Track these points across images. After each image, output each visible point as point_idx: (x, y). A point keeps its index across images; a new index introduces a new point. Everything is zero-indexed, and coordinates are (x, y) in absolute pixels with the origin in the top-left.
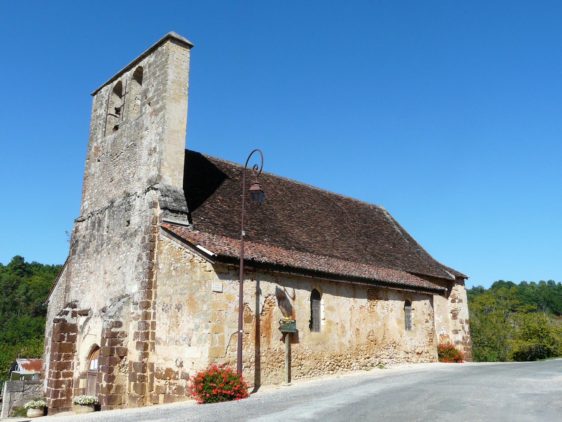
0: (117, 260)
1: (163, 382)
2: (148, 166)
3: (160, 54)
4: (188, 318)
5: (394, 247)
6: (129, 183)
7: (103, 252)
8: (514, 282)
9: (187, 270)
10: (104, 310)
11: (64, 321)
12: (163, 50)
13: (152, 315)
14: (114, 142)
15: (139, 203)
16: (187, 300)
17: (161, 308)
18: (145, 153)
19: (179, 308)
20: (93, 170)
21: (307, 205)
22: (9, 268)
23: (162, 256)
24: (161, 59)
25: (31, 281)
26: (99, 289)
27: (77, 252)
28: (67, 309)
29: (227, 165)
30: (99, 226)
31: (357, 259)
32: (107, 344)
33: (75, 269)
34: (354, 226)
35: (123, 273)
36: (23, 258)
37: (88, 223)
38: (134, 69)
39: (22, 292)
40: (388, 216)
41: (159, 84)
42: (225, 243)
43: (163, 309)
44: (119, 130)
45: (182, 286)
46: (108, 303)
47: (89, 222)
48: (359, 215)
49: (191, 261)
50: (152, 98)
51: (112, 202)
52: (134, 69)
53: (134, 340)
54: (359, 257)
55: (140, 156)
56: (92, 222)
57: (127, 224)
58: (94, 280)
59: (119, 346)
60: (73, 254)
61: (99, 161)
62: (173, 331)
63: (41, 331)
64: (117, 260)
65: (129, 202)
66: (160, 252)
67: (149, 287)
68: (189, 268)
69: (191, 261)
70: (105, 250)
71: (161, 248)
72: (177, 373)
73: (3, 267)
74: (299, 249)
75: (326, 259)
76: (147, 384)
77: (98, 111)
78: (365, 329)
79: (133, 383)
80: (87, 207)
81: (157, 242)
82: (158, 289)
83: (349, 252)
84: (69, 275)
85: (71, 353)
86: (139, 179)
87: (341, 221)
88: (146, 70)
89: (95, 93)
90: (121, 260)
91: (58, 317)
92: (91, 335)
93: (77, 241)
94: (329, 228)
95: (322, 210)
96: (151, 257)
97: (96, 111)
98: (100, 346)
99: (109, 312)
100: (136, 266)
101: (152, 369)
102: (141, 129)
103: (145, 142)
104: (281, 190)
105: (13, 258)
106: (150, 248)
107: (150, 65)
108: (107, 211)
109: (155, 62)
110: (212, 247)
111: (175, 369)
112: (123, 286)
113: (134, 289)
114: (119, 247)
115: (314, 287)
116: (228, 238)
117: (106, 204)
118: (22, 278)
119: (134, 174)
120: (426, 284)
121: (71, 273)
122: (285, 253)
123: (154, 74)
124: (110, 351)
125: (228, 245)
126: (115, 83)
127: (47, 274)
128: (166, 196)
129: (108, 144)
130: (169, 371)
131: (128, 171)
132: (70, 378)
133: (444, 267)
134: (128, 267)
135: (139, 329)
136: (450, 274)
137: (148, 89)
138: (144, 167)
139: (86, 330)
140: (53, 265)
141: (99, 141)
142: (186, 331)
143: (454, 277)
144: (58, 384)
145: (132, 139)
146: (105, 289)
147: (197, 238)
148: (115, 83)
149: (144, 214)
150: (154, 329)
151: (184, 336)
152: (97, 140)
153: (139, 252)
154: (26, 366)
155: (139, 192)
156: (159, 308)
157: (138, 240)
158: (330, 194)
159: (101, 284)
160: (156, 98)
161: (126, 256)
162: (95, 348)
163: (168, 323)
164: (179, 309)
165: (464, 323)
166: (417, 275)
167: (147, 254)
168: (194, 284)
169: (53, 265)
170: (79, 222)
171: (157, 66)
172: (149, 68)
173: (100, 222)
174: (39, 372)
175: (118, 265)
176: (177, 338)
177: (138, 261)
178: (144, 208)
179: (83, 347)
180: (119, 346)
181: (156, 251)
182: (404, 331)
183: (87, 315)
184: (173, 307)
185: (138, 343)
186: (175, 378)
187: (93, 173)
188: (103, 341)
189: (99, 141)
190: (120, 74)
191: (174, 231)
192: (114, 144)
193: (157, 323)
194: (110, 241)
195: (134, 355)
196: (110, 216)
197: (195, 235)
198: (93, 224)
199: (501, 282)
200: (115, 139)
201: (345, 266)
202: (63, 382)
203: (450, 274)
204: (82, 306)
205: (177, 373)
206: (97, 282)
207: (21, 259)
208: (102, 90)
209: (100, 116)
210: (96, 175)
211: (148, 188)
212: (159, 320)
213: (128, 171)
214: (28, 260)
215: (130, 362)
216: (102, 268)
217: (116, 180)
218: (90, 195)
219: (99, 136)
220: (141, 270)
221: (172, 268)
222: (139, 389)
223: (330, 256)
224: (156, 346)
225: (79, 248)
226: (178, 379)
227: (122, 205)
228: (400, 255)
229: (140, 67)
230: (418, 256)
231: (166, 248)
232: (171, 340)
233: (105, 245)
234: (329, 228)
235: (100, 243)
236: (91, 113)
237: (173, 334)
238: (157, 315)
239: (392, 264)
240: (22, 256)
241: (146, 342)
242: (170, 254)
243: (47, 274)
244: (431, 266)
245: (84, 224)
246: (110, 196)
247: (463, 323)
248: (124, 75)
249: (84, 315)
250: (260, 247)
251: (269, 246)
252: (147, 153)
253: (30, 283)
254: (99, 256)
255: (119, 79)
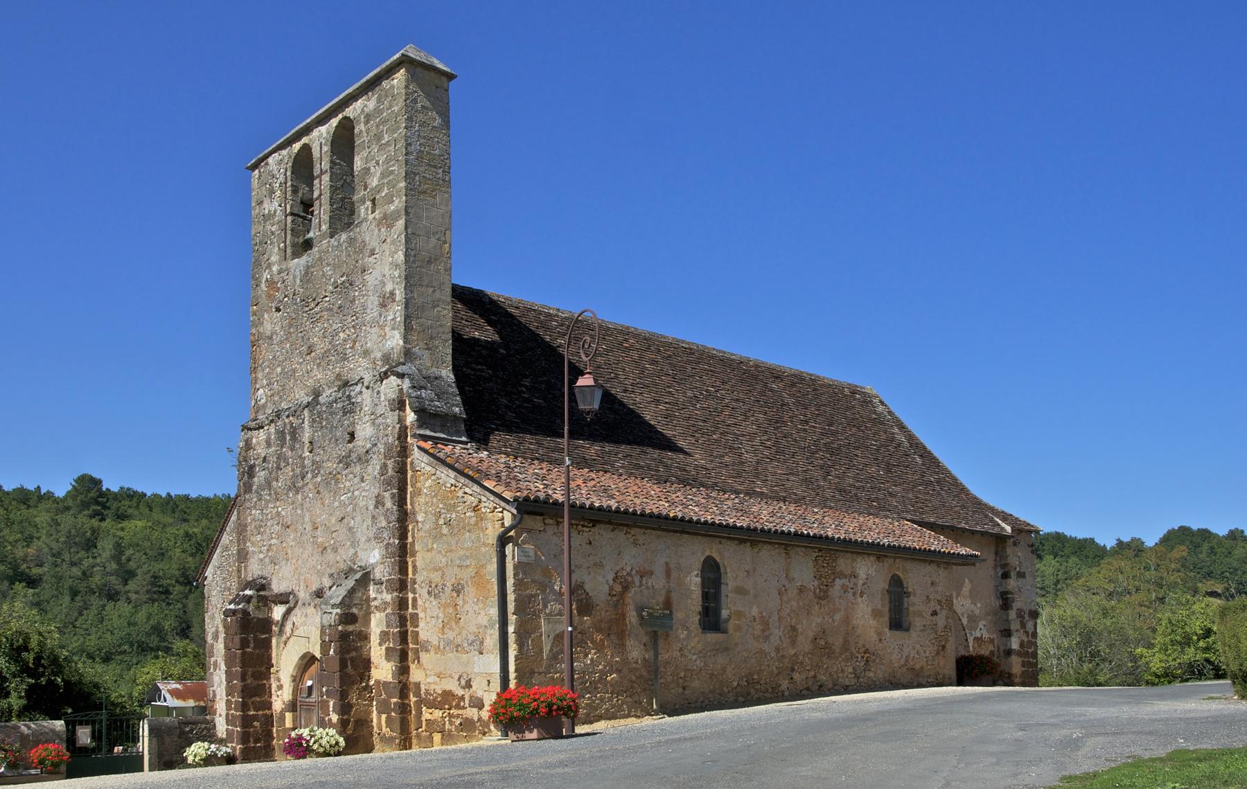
0: (336, 504)
1: (438, 714)
2: (382, 327)
3: (387, 96)
4: (476, 608)
5: (888, 470)
6: (345, 358)
7: (306, 489)
8: (1213, 530)
9: (469, 524)
10: (319, 594)
11: (245, 613)
12: (393, 87)
13: (410, 602)
14: (307, 273)
15: (369, 400)
16: (472, 578)
17: (425, 591)
18: (373, 301)
19: (458, 590)
20: (267, 328)
21: (707, 391)
22: (70, 502)
23: (422, 499)
24: (391, 106)
25: (123, 529)
26: (305, 556)
27: (255, 487)
28: (248, 592)
29: (541, 313)
30: (294, 438)
31: (804, 498)
32: (331, 652)
33: (253, 520)
34: (805, 430)
35: (350, 529)
36: (100, 482)
37: (269, 434)
38: (334, 122)
39: (106, 554)
40: (880, 408)
41: (390, 160)
42: (537, 474)
43: (429, 593)
44: (315, 249)
45: (462, 553)
46: (327, 582)
47: (273, 430)
48: (818, 407)
49: (476, 509)
50: (378, 189)
51: (317, 394)
52: (334, 122)
53: (380, 644)
54: (812, 494)
55: (364, 308)
56: (277, 432)
57: (347, 437)
58: (294, 540)
59: (354, 654)
60: (245, 492)
61: (278, 310)
62: (451, 628)
63: (189, 627)
64: (336, 504)
65: (349, 397)
66: (418, 492)
67: (402, 553)
68: (473, 520)
69: (476, 509)
70: (310, 486)
71: (418, 485)
72: (462, 698)
73: (57, 501)
74: (684, 482)
75: (737, 501)
76: (412, 717)
77: (265, 205)
78: (809, 626)
79: (384, 716)
80: (263, 401)
81: (410, 473)
82: (419, 557)
83: (789, 484)
84: (241, 529)
85: (263, 669)
86: (366, 353)
87: (777, 422)
88: (360, 128)
89: (255, 166)
90: (343, 505)
91: (232, 606)
92: (300, 639)
93: (252, 467)
94: (752, 436)
95: (737, 400)
96: (401, 500)
97: (260, 203)
98: (318, 655)
99: (331, 598)
100: (373, 517)
101: (418, 694)
102: (361, 251)
103: (372, 279)
104: (654, 362)
105: (76, 481)
106: (400, 483)
107: (368, 118)
108: (306, 412)
109: (378, 111)
110: (513, 483)
111: (460, 692)
112: (352, 551)
113: (374, 557)
114: (337, 481)
115: (708, 554)
116: (544, 465)
117: (303, 397)
118: (104, 524)
119: (355, 342)
120: (938, 543)
121: (246, 526)
122: (654, 490)
123: (378, 137)
124: (346, 657)
125: (544, 479)
126: (297, 146)
127: (157, 515)
128: (421, 388)
129: (294, 277)
130: (447, 695)
131: (342, 335)
132: (267, 712)
133: (992, 509)
134: (358, 519)
135: (388, 626)
136: (1003, 525)
137: (369, 169)
138: (374, 330)
139: (288, 628)
140: (169, 494)
141: (275, 268)
142: (473, 629)
143: (1008, 529)
144: (246, 722)
145: (344, 270)
146: (317, 557)
147: (484, 467)
148: (297, 146)
149: (380, 420)
150: (417, 626)
151: (471, 638)
152: (269, 266)
153: (376, 491)
154: (175, 693)
155: (368, 378)
156: (422, 592)
157: (374, 468)
158: (757, 366)
159: (309, 548)
160: (386, 191)
161: (353, 498)
162: (308, 661)
163: (441, 615)
164: (458, 592)
165: (1026, 616)
166: (931, 526)
167: (393, 496)
168: (483, 549)
169: (169, 494)
170: (250, 429)
171: (384, 122)
172: (367, 122)
173: (295, 432)
174: (202, 704)
175: (339, 514)
176: (459, 640)
177: (376, 507)
178: (380, 411)
179: (285, 660)
180: (354, 654)
181: (410, 489)
182: (887, 630)
183: (287, 602)
184: (448, 590)
185: (387, 649)
186: (458, 707)
187: (268, 333)
188: (325, 647)
189: (275, 268)
190: (307, 130)
191: (441, 455)
192: (307, 276)
193: (421, 615)
194: (318, 468)
195: (382, 670)
196: (314, 421)
197: (481, 461)
198: (281, 434)
199: (1184, 530)
200: (308, 267)
201: (772, 514)
202: (255, 718)
203: (1003, 525)
204: (278, 587)
205: (462, 698)
206: (300, 544)
207: (98, 483)
208: (270, 160)
209: (271, 216)
210: (276, 339)
211: (385, 373)
212: (425, 610)
213: (342, 335)
214: (111, 484)
215: (378, 682)
216: (307, 519)
217: (319, 351)
218: (268, 376)
219: (274, 258)
220: (384, 524)
221: (441, 521)
222: (397, 725)
223: (747, 494)
224: (423, 655)
225: (256, 479)
226: (464, 708)
227: (336, 401)
228: (898, 489)
229: (346, 118)
230: (938, 488)
231: (427, 484)
232: (449, 643)
233: (309, 475)
234: (752, 436)
235: (298, 471)
236: (250, 208)
237: (450, 635)
238: (420, 602)
239: (879, 508)
240: (96, 475)
241: (404, 649)
242: (436, 496)
243: (157, 515)
244: (963, 507)
245: (262, 435)
246: (310, 382)
247: (1023, 617)
248: (315, 133)
249: (282, 603)
250: (606, 480)
251: (624, 477)
252: (377, 303)
253: (120, 533)
254: (299, 497)
255: (305, 140)
